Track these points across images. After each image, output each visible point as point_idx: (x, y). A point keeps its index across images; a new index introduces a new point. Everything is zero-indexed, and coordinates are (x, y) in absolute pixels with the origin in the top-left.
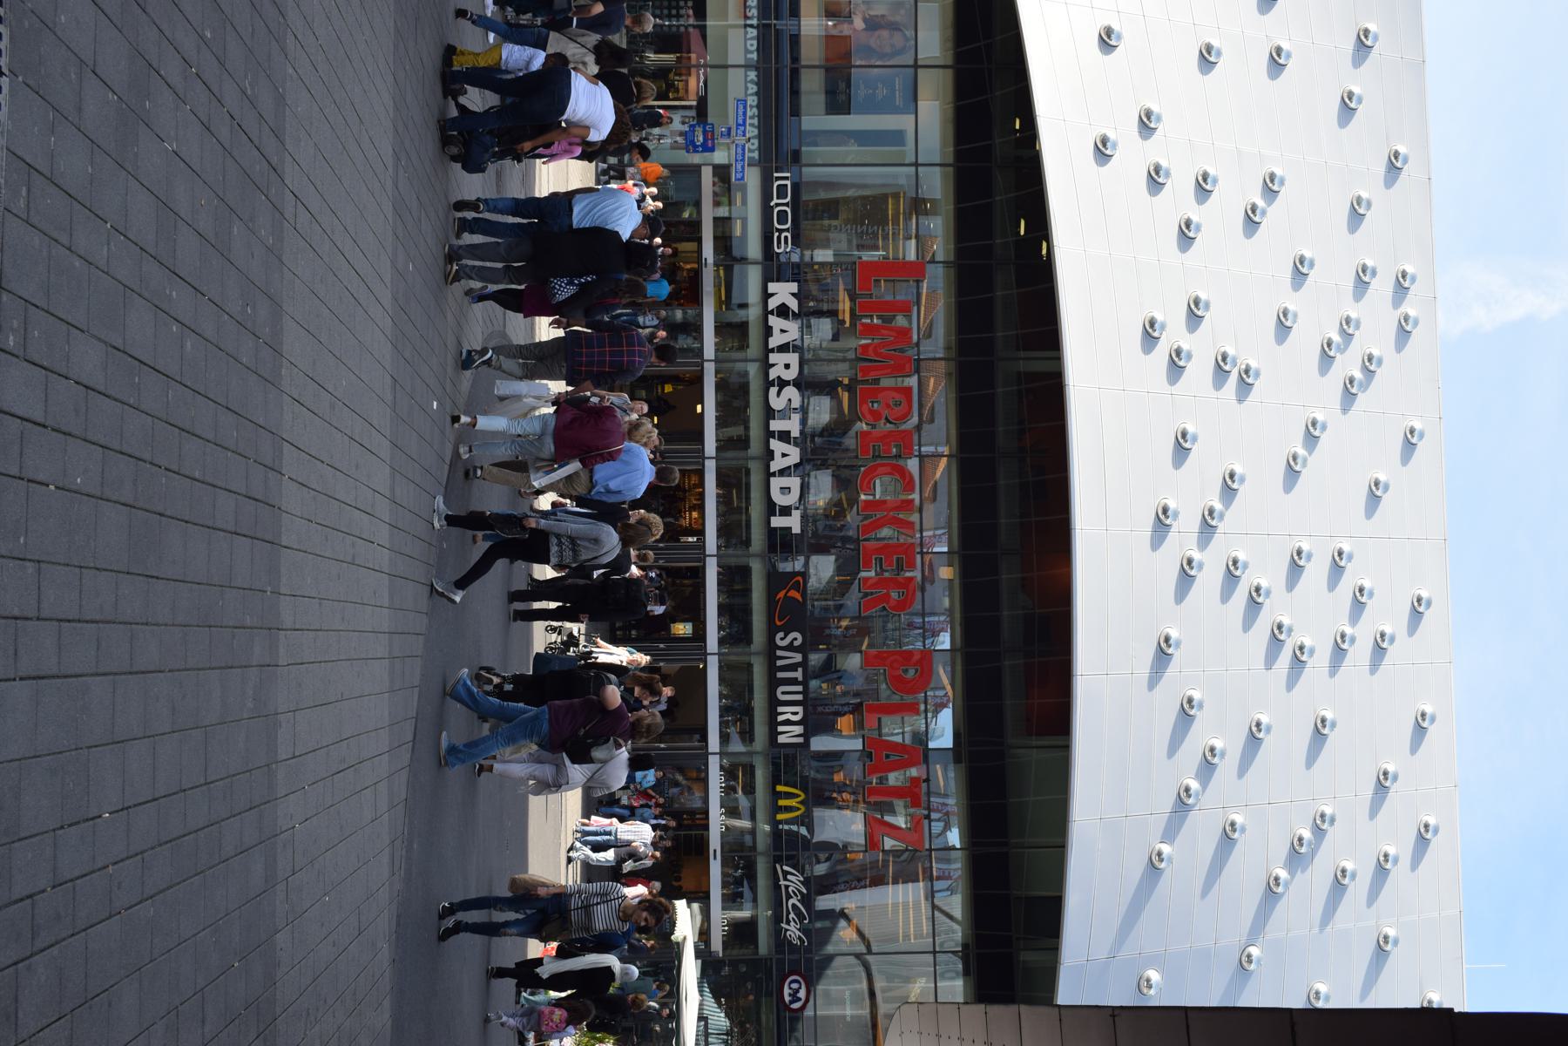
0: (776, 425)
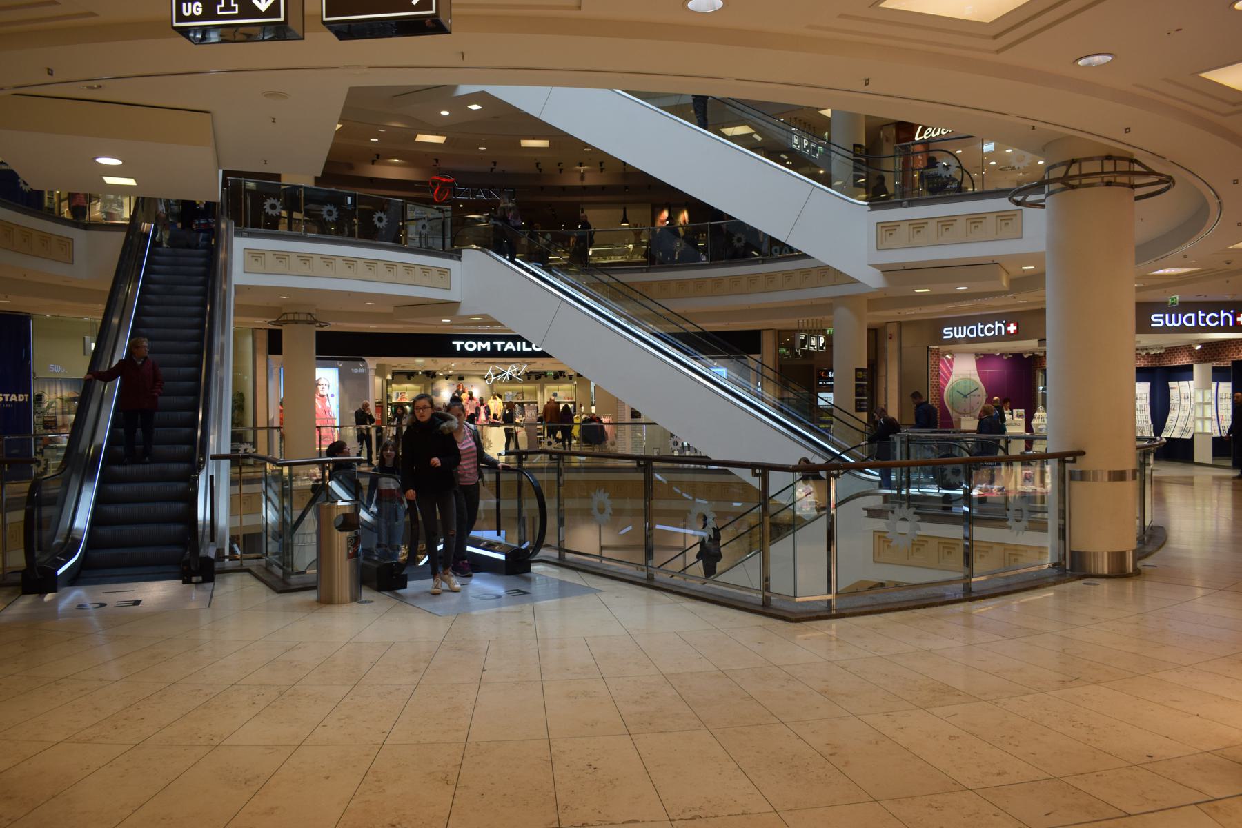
0: (7, 400)
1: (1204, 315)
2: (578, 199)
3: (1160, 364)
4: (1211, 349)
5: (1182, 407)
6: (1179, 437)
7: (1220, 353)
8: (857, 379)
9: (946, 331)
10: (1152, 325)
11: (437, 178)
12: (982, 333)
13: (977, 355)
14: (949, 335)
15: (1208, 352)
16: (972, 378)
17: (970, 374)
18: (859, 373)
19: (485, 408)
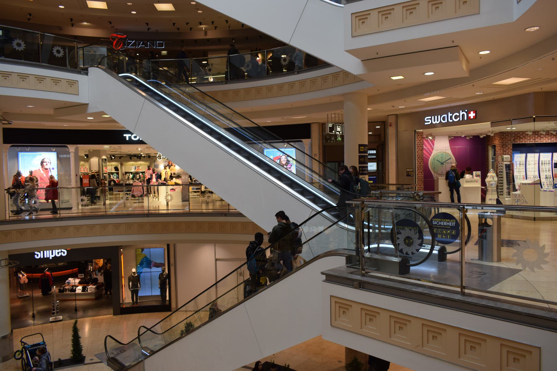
2: (206, 48)
8: (360, 152)
9: (427, 119)
11: (115, 35)
12: (451, 119)
13: (449, 137)
14: (429, 122)
16: (446, 151)
17: (445, 150)
18: (361, 147)
19: (156, 174)
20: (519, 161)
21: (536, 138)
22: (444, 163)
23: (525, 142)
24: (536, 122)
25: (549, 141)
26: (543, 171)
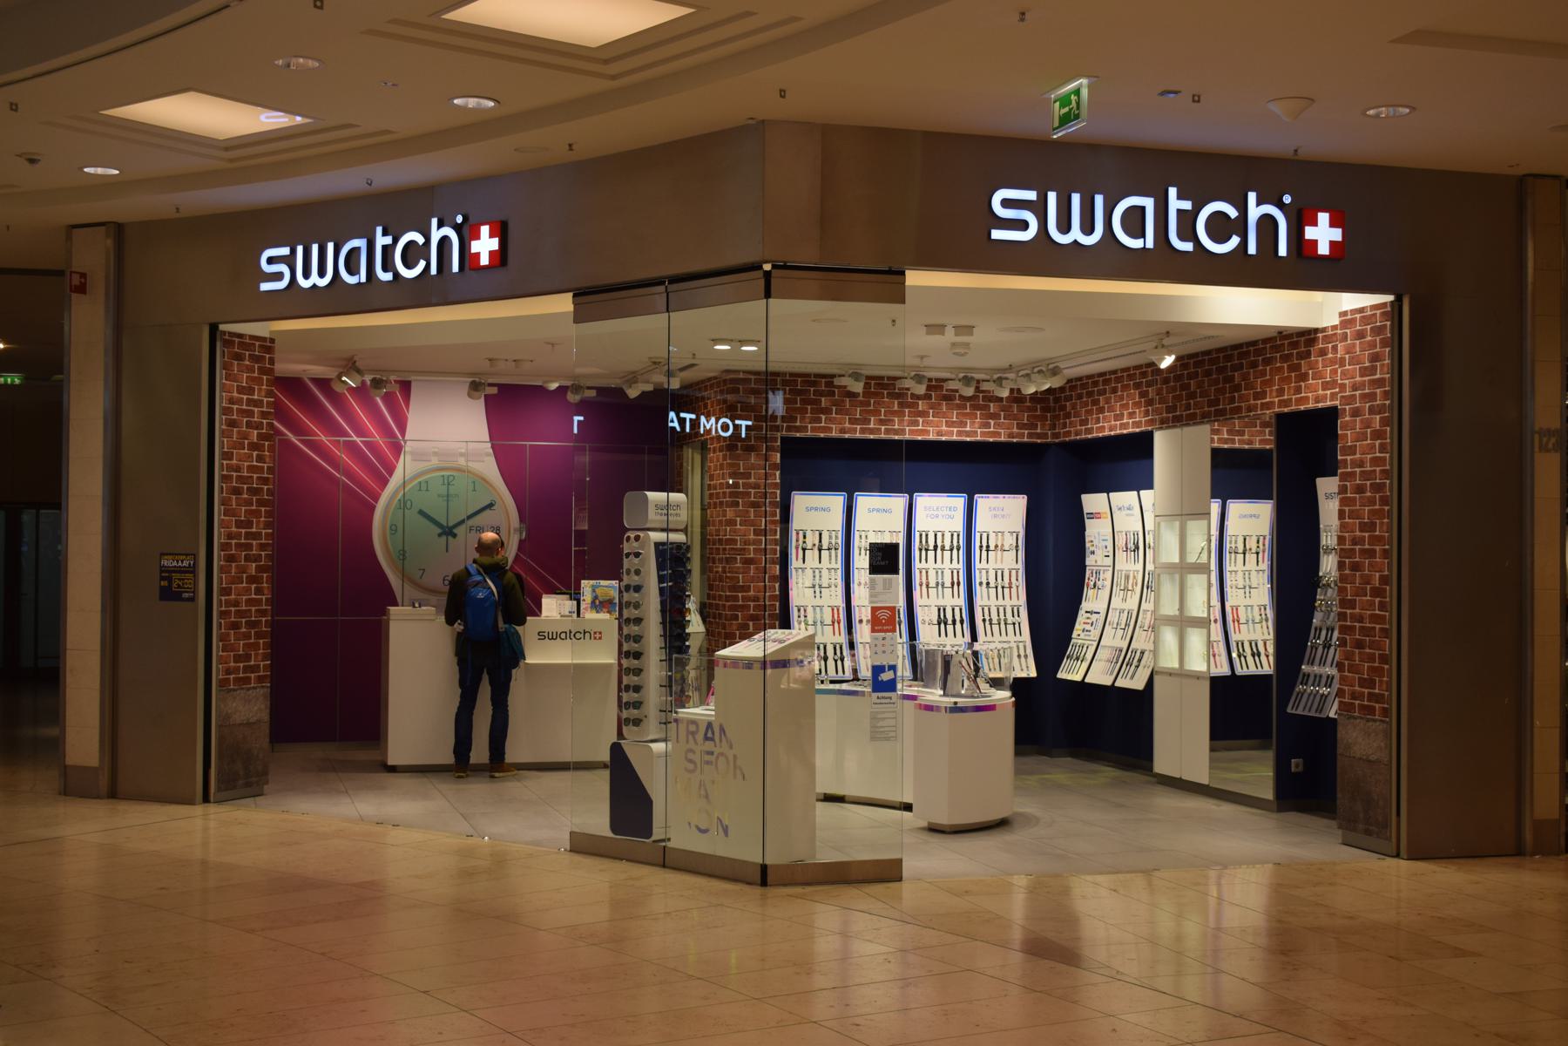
1: (1187, 205)
3: (1056, 435)
4: (1208, 373)
5: (1118, 578)
6: (1109, 683)
7: (1237, 388)
10: (997, 234)
12: (385, 269)
15: (1200, 385)
20: (1012, 533)
21: (894, 413)
22: (460, 531)
23: (843, 431)
24: (774, 298)
25: (952, 433)
26: (927, 586)
